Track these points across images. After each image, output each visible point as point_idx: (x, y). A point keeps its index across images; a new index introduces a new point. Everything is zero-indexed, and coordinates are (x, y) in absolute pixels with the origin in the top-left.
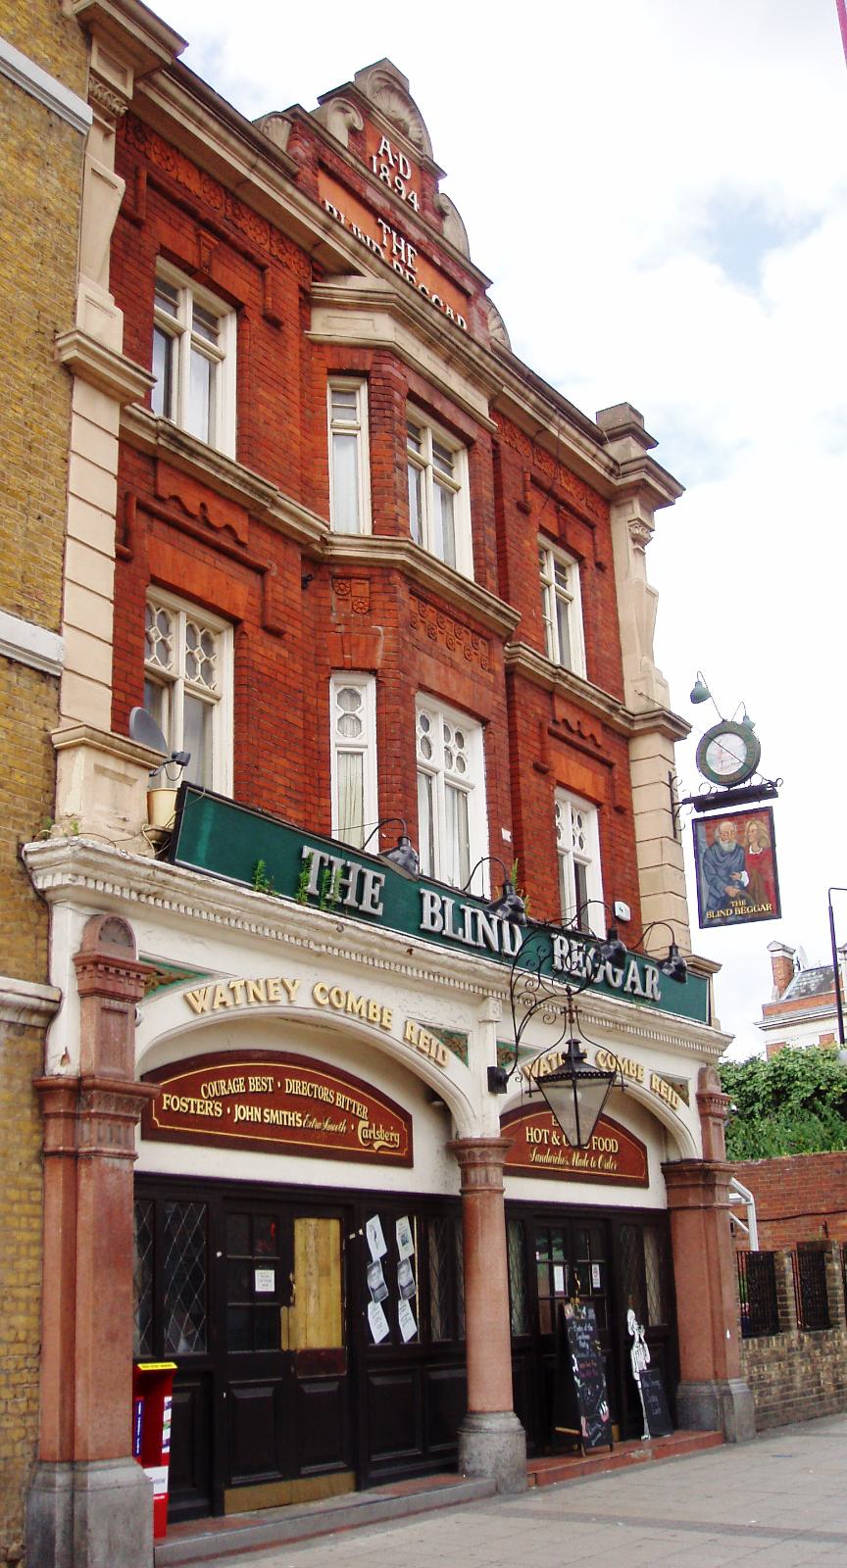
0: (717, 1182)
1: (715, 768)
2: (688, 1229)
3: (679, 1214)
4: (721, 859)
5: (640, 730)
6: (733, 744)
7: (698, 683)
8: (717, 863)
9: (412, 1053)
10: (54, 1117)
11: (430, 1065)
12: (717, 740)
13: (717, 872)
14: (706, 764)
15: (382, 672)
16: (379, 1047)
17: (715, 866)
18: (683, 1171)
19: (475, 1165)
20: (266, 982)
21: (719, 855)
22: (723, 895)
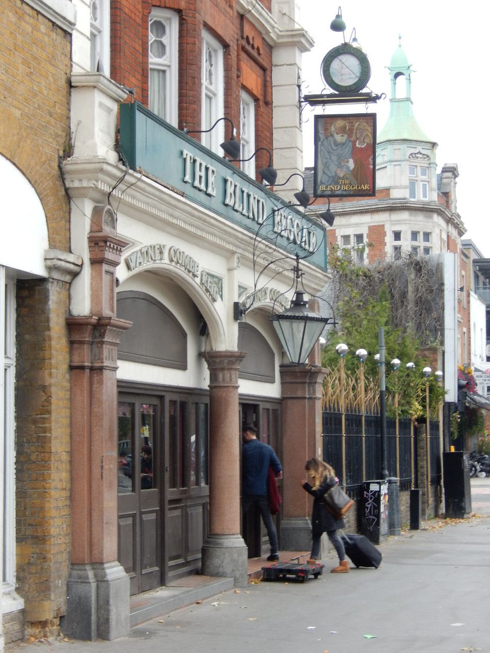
0: (318, 381)
1: (337, 80)
2: (293, 410)
3: (289, 402)
4: (335, 148)
5: (283, 43)
6: (351, 62)
7: (338, 16)
8: (331, 150)
9: (201, 291)
10: (78, 343)
11: (206, 298)
12: (340, 57)
13: (330, 157)
14: (329, 76)
15: (186, 12)
16: (187, 291)
17: (329, 152)
18: (296, 372)
19: (223, 369)
20: (154, 247)
21: (333, 145)
22: (334, 174)
